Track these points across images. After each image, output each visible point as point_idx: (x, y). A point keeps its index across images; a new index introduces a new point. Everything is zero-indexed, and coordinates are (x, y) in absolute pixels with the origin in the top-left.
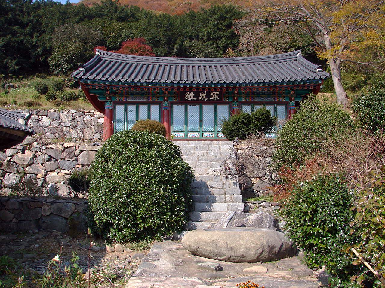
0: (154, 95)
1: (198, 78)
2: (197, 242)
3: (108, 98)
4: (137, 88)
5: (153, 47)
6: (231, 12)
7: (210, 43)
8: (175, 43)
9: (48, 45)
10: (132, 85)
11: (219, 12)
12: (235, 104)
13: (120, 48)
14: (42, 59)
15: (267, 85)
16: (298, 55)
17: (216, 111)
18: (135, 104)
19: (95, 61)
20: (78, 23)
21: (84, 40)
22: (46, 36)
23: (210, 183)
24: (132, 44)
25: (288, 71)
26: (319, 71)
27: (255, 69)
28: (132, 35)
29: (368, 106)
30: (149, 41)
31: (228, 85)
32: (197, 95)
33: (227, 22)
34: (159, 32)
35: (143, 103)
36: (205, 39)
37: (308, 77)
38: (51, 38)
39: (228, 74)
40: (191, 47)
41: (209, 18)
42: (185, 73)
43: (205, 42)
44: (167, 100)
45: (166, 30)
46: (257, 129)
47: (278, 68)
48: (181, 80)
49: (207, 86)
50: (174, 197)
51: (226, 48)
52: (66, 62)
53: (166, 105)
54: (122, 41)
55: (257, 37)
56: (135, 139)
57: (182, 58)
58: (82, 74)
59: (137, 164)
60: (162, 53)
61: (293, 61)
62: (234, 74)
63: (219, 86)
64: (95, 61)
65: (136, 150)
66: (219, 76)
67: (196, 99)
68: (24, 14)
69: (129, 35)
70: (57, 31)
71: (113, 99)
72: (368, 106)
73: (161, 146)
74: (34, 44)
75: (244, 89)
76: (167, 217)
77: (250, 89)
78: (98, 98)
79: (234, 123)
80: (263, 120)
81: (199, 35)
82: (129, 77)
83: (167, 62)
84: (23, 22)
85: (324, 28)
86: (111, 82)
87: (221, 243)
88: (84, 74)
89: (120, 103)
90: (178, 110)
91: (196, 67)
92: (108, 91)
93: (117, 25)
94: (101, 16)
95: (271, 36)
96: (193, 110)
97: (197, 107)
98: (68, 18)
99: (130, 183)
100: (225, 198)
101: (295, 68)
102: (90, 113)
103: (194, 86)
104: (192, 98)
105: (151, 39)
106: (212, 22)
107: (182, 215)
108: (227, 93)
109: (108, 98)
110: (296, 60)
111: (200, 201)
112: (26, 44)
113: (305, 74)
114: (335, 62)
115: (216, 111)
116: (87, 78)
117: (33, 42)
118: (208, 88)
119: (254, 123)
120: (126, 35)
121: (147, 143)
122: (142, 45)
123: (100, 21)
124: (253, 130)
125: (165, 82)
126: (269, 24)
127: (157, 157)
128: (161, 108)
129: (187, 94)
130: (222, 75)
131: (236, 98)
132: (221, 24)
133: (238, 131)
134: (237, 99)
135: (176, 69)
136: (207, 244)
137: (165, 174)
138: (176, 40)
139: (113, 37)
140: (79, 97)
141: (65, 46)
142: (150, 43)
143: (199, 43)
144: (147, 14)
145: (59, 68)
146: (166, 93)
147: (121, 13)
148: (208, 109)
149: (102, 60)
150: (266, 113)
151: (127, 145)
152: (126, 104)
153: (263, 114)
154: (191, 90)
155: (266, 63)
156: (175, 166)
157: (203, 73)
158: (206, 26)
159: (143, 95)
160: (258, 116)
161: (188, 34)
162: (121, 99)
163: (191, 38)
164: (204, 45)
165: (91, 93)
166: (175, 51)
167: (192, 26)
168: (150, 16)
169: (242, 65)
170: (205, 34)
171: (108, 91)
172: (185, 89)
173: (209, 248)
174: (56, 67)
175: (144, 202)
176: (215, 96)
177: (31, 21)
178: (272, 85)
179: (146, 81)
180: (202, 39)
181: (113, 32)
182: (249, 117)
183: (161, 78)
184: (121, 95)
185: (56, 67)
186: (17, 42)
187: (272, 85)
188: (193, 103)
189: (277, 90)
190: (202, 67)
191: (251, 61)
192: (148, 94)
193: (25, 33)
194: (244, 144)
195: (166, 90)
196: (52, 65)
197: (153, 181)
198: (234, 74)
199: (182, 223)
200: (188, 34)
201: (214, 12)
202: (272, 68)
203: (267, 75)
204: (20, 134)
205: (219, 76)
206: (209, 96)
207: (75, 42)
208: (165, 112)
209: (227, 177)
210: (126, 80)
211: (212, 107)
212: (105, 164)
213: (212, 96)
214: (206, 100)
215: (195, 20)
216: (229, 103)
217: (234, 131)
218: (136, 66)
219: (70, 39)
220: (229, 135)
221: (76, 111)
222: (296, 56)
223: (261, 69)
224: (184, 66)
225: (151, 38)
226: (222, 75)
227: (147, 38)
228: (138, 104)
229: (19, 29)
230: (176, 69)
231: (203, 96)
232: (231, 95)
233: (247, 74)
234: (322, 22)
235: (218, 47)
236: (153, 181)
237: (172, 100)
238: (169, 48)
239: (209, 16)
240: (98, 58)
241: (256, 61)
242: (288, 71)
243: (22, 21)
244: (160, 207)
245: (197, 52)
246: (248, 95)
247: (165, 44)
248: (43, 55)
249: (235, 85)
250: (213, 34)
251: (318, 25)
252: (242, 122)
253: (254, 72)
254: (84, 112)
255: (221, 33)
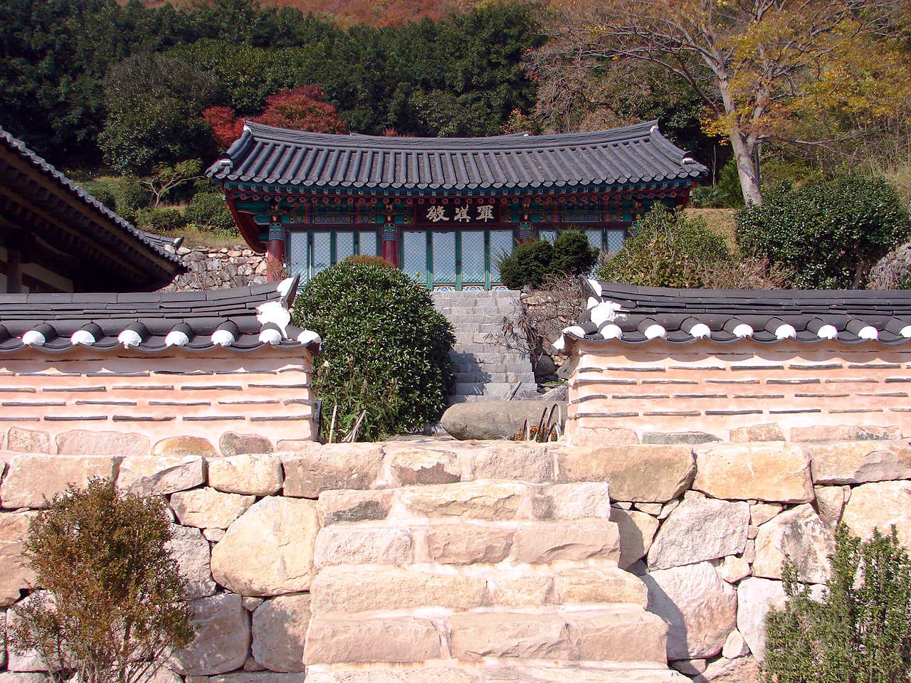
0: (365, 212)
1: (452, 178)
2: (464, 417)
3: (275, 219)
4: (322, 198)
5: (340, 107)
6: (518, 24)
7: (470, 96)
8: (390, 96)
9: (93, 103)
10: (314, 192)
11: (491, 23)
12: (525, 229)
13: (261, 112)
14: (81, 135)
15: (586, 191)
16: (652, 130)
17: (487, 242)
18: (328, 231)
19: (245, 145)
20: (160, 50)
21: (181, 92)
22: (88, 82)
23: (479, 356)
24: (293, 102)
25: (628, 162)
26: (686, 163)
27: (563, 159)
28: (289, 80)
29: (760, 224)
30: (329, 92)
31: (511, 191)
32: (450, 212)
33: (508, 49)
34: (352, 72)
35: (344, 228)
36: (459, 86)
37: (665, 173)
38: (99, 87)
39: (511, 170)
40: (426, 107)
41: (469, 37)
42: (427, 169)
43: (458, 95)
44: (392, 221)
45: (368, 68)
46: (564, 269)
47: (609, 157)
48: (419, 182)
49: (470, 194)
50: (426, 366)
51: (507, 108)
52: (142, 142)
53: (389, 231)
54: (268, 94)
55: (574, 86)
56: (361, 275)
57: (419, 139)
58: (227, 170)
59: (366, 314)
60: (359, 122)
61: (642, 142)
62: (522, 168)
63: (493, 194)
64: (245, 145)
65: (362, 292)
66: (494, 174)
67: (447, 219)
68: (33, 28)
69: (284, 79)
70: (116, 71)
71: (285, 221)
72: (760, 224)
73: (403, 286)
74: (62, 99)
75: (542, 199)
76: (415, 395)
77: (554, 199)
78: (254, 218)
79: (522, 259)
80: (575, 253)
81: (444, 78)
82: (282, 175)
83: (388, 146)
84: (33, 47)
85: (719, 66)
86: (259, 185)
87: (501, 416)
88: (232, 171)
89: (299, 228)
90: (413, 242)
91: (448, 156)
92: (276, 203)
93: (253, 56)
94: (213, 33)
95: (607, 83)
96: (444, 241)
97: (451, 235)
98: (137, 39)
99: (357, 342)
100: (507, 377)
101: (662, 159)
102: (219, 255)
103: (446, 194)
104: (441, 217)
105: (334, 89)
106: (476, 46)
107: (438, 395)
108: (509, 208)
109: (275, 219)
110: (647, 141)
111: (463, 381)
112: (41, 99)
113: (660, 168)
114: (744, 140)
115: (487, 242)
116: (239, 179)
117: (58, 96)
118: (473, 198)
119: (559, 259)
120: (274, 81)
121: (379, 282)
122: (313, 103)
123: (214, 46)
124: (556, 272)
125: (390, 186)
126: (602, 58)
127: (397, 302)
128: (379, 237)
129: (431, 210)
130: (499, 171)
131: (526, 217)
132: (497, 52)
133: (530, 275)
134: (529, 219)
135: (407, 161)
136: (479, 419)
137: (411, 328)
138: (393, 90)
139: (245, 85)
140: (187, 222)
141: (136, 106)
142: (332, 98)
143: (446, 97)
144: (321, 29)
145: (125, 158)
146: (389, 209)
147: (261, 25)
148: (472, 240)
149: (257, 142)
150: (579, 241)
151: (348, 285)
152: (310, 230)
153: (574, 241)
154: (438, 202)
155: (587, 147)
156: (426, 317)
157: (462, 168)
158: (460, 57)
159: (343, 212)
160: (565, 245)
161: (419, 76)
162: (300, 220)
163: (427, 87)
164: (456, 103)
165: (241, 209)
166: (391, 117)
167: (429, 57)
168: (327, 32)
169: (539, 152)
170: (460, 74)
171: (276, 203)
172: (427, 201)
173: (483, 426)
174: (118, 155)
175: (379, 370)
176: (486, 213)
177: (50, 45)
178: (596, 190)
179: (352, 185)
180: (452, 87)
181: (244, 73)
182: (550, 247)
183: (345, 177)
184: (300, 212)
185: (118, 155)
186: (19, 95)
187: (596, 190)
188: (442, 227)
189: (606, 199)
190: (459, 156)
191: (557, 144)
192: (355, 212)
193: (38, 74)
194: (538, 297)
195: (391, 200)
196: (109, 148)
197: (392, 338)
198: (522, 168)
199: (438, 408)
200: (419, 76)
201: (479, 22)
202: (597, 157)
203: (585, 170)
204: (169, 268)
205: (494, 174)
206: (473, 213)
207: (160, 97)
208: (388, 246)
209: (509, 347)
210: (315, 183)
211: (480, 235)
212: (310, 316)
213: (480, 214)
214: (468, 221)
215: (435, 42)
216: (514, 228)
217: (521, 274)
218: (328, 155)
219: (148, 88)
220: (513, 281)
221: (189, 251)
222: (647, 132)
223: (576, 160)
224: (411, 154)
225: (334, 86)
226: (499, 171)
227: (324, 86)
228: (333, 230)
229: (23, 64)
230: (373, 160)
231: (462, 214)
232: (517, 211)
233: (547, 170)
234: (715, 54)
235: (490, 106)
236: (392, 338)
237: (401, 222)
238: (375, 108)
239: (467, 33)
240: (249, 139)
241: (567, 143)
242: (628, 162)
243: (29, 44)
244: (404, 381)
245: (441, 118)
246: (549, 210)
247: (365, 100)
248: (81, 125)
249: (524, 191)
250: (478, 75)
251: (708, 61)
252: (536, 258)
253: (562, 165)
254: (208, 252)
255: (495, 75)
